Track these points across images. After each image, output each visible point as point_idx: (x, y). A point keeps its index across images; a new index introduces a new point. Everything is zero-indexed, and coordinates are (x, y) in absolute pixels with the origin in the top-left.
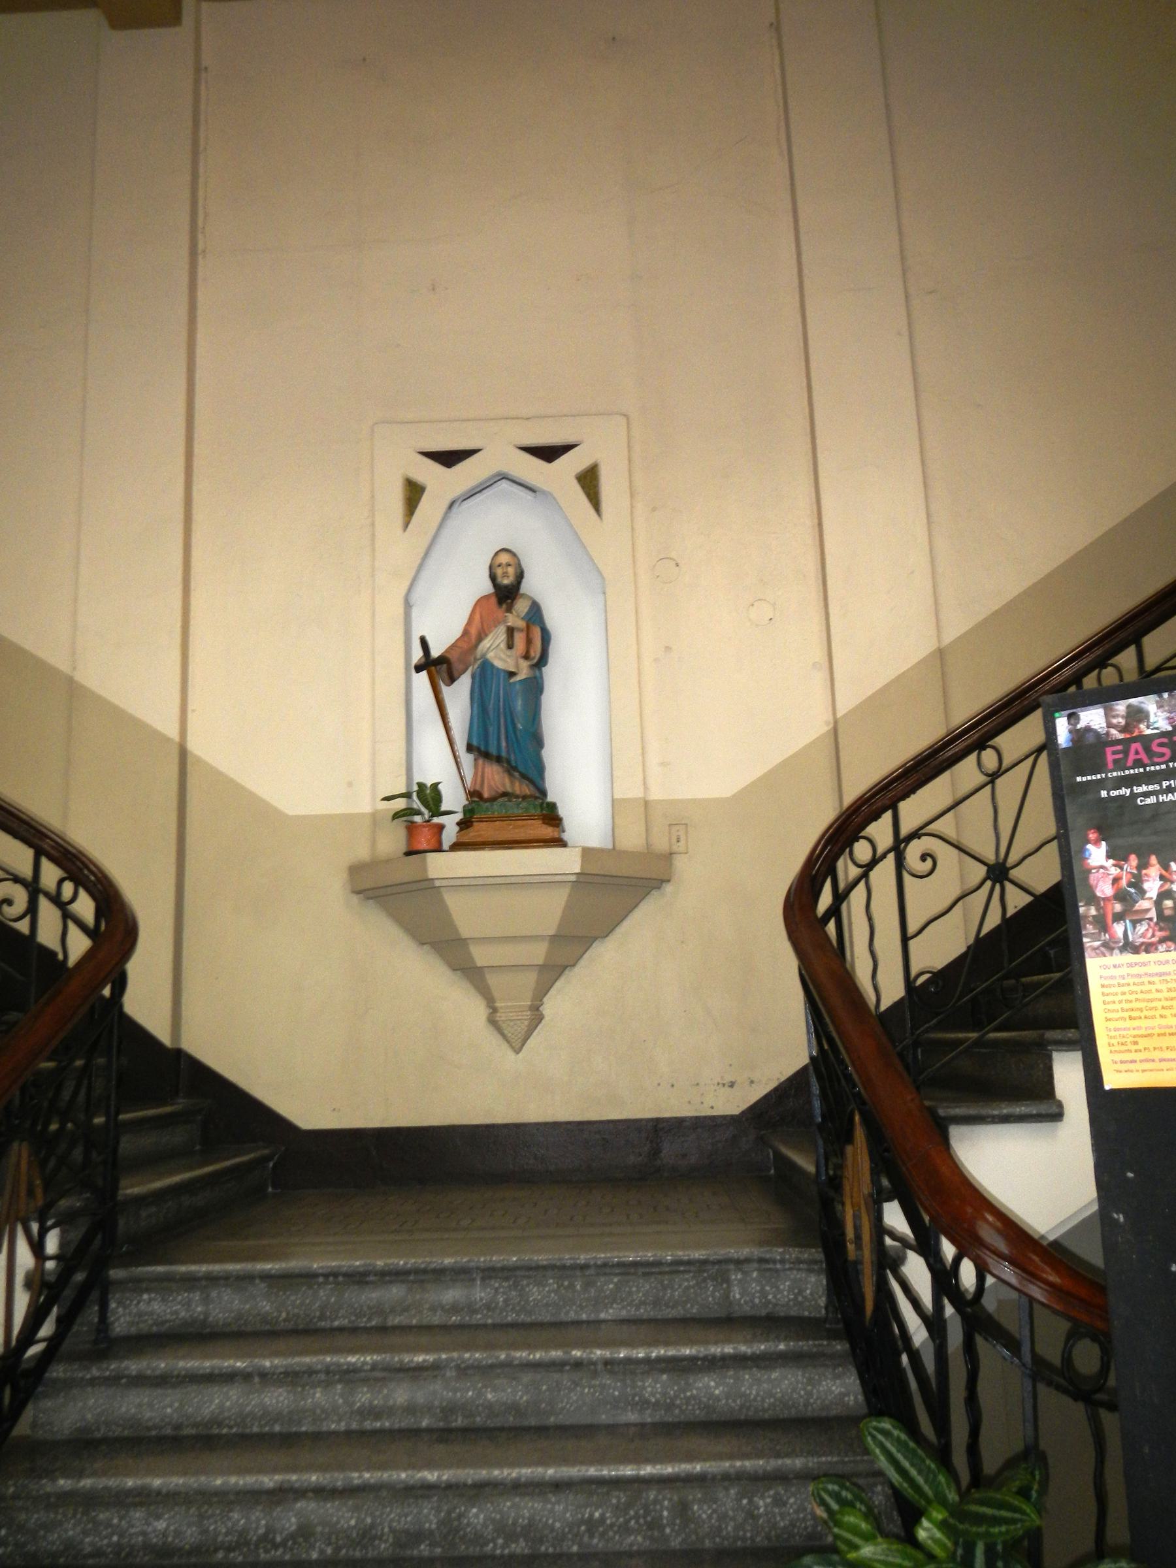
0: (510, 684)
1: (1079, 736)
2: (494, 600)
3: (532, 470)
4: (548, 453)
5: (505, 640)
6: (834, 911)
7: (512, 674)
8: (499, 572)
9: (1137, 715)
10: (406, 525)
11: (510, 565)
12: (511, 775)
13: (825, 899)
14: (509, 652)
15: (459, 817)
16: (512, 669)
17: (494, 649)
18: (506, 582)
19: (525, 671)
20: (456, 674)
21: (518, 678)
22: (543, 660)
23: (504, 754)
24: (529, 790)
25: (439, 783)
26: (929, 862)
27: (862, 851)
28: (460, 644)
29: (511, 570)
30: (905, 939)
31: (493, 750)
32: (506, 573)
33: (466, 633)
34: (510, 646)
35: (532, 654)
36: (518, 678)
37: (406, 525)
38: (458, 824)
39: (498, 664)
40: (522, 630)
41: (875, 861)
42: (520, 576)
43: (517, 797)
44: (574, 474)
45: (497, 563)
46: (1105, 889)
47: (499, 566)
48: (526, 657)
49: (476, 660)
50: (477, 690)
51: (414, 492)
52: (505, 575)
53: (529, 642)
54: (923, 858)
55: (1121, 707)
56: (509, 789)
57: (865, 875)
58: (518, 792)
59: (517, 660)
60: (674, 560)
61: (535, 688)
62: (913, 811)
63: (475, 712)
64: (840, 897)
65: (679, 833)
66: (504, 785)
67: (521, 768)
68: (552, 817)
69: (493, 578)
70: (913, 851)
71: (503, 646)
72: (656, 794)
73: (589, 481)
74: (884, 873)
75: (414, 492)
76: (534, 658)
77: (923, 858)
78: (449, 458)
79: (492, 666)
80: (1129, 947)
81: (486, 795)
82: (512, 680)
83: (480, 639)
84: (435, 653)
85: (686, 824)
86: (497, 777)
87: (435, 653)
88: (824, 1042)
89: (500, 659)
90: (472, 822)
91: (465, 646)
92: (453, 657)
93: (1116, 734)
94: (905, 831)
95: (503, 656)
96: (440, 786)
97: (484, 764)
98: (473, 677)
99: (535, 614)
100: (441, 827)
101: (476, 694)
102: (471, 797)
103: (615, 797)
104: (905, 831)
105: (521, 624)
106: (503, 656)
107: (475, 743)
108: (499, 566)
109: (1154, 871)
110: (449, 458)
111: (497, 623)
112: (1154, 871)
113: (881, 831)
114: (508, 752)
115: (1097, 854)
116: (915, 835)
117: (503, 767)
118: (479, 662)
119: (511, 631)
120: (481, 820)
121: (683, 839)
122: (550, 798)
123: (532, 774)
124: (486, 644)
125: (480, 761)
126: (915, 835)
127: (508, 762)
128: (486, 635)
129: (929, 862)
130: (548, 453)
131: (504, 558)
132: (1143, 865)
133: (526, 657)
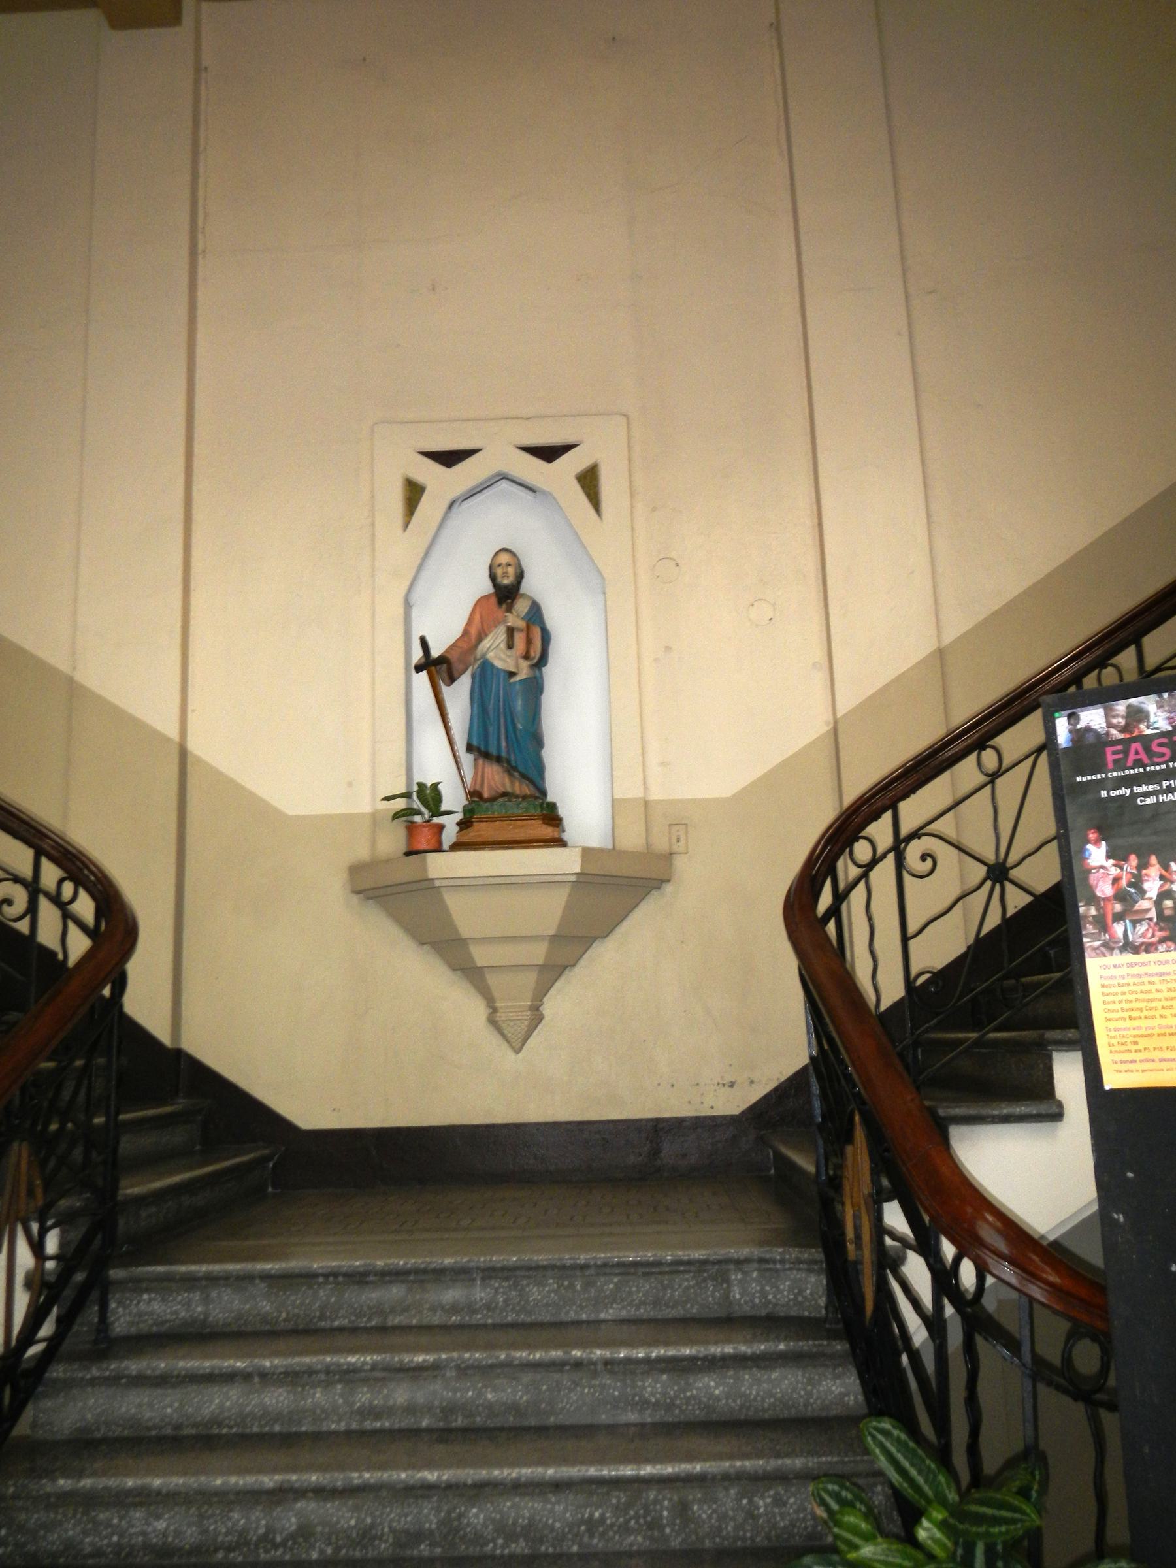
0: (510, 684)
1: (1079, 736)
2: (494, 600)
3: (532, 470)
4: (548, 453)
5: (505, 640)
6: (834, 911)
7: (512, 674)
8: (499, 572)
9: (1137, 715)
10: (406, 525)
11: (510, 565)
12: (511, 775)
13: (825, 899)
14: (509, 652)
15: (459, 817)
16: (512, 669)
17: (494, 649)
18: (506, 582)
19: (525, 671)
20: (456, 674)
21: (518, 678)
22: (543, 660)
23: (504, 754)
24: (529, 790)
25: (439, 783)
26: (929, 862)
27: (862, 851)
28: (460, 644)
29: (511, 570)
30: (905, 939)
31: (493, 750)
32: (506, 573)
33: (466, 633)
34: (510, 646)
35: (532, 654)
36: (518, 678)
37: (406, 525)
38: (458, 824)
39: (498, 664)
40: (522, 630)
41: (875, 861)
42: (520, 576)
43: (517, 797)
44: (574, 474)
45: (497, 563)
46: (1105, 889)
47: (499, 566)
48: (526, 657)
49: (476, 660)
50: (477, 690)
51: (414, 492)
52: (505, 575)
53: (529, 642)
54: (923, 858)
55: (1121, 707)
56: (509, 789)
57: (865, 875)
58: (518, 792)
59: (517, 660)
60: (674, 560)
61: (535, 688)
62: (913, 811)
63: (475, 712)
64: (840, 897)
65: (679, 833)
66: (504, 785)
67: (521, 768)
68: (552, 817)
69: (493, 578)
70: (913, 851)
71: (503, 646)
72: (656, 794)
73: (589, 481)
74: (884, 873)
75: (414, 492)
76: (534, 658)
77: (923, 858)
78: (449, 458)
79: (492, 666)
80: (1129, 947)
81: (486, 795)
82: (512, 680)
83: (480, 639)
84: (435, 653)
85: (686, 824)
86: (497, 777)
87: (435, 653)
88: (824, 1042)
89: (500, 659)
90: (472, 822)
91: (465, 646)
92: (453, 657)
93: (1116, 734)
94: (905, 831)
95: (503, 656)
96: (440, 786)
97: (484, 764)
98: (473, 677)
99: (535, 614)
100: (441, 827)
101: (476, 694)
102: (471, 797)
103: (615, 797)
104: (905, 831)
105: (521, 624)
106: (503, 656)
107: (475, 743)
108: (499, 566)
109: (1154, 871)
110: (449, 458)
111: (497, 623)
112: (1154, 871)
113: (881, 831)
114: (508, 752)
115: (1097, 854)
116: (915, 835)
117: (503, 767)
118: (479, 662)
119: (511, 631)
120: (481, 820)
121: (683, 839)
122: (550, 798)
123: (532, 774)
124: (486, 644)
125: (480, 761)
126: (915, 835)
127: (508, 762)
128: (486, 635)
129: (929, 862)
130: (548, 453)
131: (504, 558)
132: (1143, 865)
133: (526, 657)
